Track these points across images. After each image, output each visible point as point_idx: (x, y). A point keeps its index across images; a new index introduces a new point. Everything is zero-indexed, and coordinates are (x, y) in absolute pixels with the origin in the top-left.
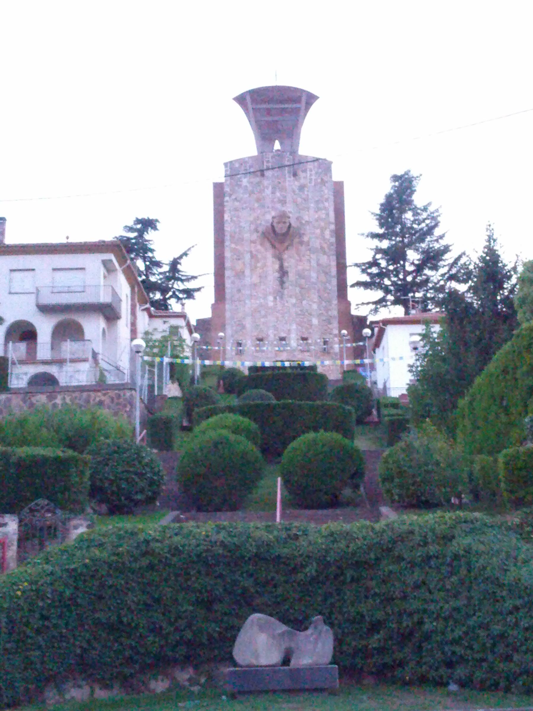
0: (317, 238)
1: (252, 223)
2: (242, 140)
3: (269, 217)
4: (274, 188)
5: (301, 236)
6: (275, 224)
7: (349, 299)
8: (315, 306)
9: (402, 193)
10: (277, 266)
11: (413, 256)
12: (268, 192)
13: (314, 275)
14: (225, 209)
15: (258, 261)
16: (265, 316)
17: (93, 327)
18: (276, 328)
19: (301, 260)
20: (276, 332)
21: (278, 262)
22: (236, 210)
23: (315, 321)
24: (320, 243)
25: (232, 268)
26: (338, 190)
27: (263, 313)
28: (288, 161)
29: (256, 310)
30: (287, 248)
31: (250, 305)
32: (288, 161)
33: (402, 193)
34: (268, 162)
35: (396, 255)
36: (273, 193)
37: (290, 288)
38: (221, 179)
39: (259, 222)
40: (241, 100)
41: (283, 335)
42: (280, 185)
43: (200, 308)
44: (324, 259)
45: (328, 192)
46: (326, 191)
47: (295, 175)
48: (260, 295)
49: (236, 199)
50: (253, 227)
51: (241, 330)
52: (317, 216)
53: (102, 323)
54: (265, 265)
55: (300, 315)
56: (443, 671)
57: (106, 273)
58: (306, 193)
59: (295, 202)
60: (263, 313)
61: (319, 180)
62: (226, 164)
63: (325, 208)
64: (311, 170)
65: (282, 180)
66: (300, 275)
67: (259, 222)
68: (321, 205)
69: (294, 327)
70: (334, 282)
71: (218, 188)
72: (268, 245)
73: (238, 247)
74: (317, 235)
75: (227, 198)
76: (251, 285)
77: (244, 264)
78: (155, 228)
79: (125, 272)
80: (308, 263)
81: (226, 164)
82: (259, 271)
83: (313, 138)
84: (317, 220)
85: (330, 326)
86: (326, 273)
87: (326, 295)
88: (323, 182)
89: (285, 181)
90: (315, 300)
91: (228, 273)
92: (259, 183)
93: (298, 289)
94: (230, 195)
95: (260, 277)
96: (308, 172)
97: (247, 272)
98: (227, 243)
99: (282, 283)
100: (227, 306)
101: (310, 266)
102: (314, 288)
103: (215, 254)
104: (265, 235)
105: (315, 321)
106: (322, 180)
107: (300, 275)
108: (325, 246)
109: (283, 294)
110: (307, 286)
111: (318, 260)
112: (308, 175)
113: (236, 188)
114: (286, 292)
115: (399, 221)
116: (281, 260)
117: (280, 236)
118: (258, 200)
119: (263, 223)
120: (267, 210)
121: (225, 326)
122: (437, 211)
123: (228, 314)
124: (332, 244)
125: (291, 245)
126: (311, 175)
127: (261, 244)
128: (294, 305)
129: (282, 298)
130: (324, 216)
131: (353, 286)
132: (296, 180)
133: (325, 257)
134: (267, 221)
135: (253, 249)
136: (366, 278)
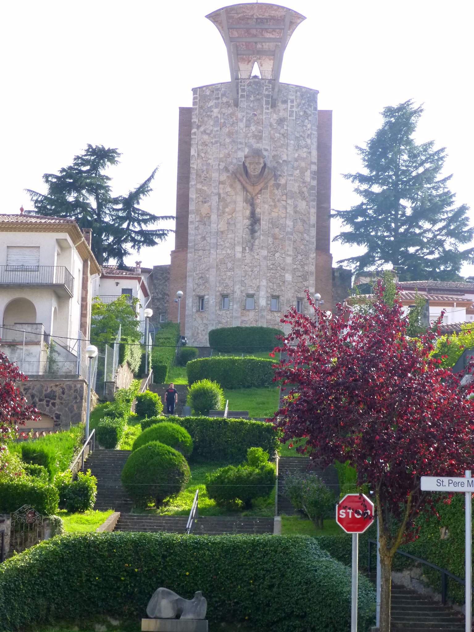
0: (295, 181)
1: (221, 160)
2: (215, 66)
3: (241, 155)
4: (248, 120)
5: (276, 177)
6: (247, 164)
7: (331, 251)
8: (289, 260)
9: (399, 123)
10: (248, 213)
11: (407, 205)
12: (242, 125)
13: (289, 223)
14: (192, 142)
15: (226, 206)
16: (232, 269)
17: (45, 306)
18: (242, 283)
19: (275, 206)
20: (243, 288)
21: (250, 208)
22: (205, 144)
23: (288, 277)
24: (299, 186)
25: (198, 212)
26: (324, 121)
27: (229, 265)
28: (267, 89)
29: (222, 262)
30: (260, 192)
31: (214, 257)
32: (267, 89)
33: (399, 123)
34: (243, 90)
35: (386, 204)
36: (247, 126)
37: (261, 238)
38: (189, 104)
39: (229, 160)
40: (214, 17)
41: (251, 292)
42: (255, 118)
43: (159, 255)
44: (302, 205)
45: (310, 127)
46: (309, 126)
47: (274, 105)
48: (227, 245)
49: (205, 131)
50: (222, 165)
51: (204, 284)
52: (296, 155)
53: (54, 304)
54: (234, 211)
55: (272, 269)
56: (449, 522)
57: (59, 251)
58: (285, 128)
59: (272, 138)
60: (229, 265)
61: (301, 113)
62: (195, 90)
63: (307, 146)
64: (292, 101)
65: (259, 111)
66: (274, 223)
67: (229, 160)
68: (302, 143)
69: (264, 283)
70: (313, 232)
71: (185, 113)
72: (239, 186)
73: (205, 188)
74: (296, 178)
75: (194, 130)
76: (217, 233)
77: (210, 206)
78: (112, 160)
79: (78, 248)
80: (283, 210)
81: (195, 90)
82: (227, 217)
83: (298, 66)
84: (296, 160)
85: (306, 284)
86: (304, 221)
87: (302, 247)
88: (306, 115)
89: (262, 113)
90: (290, 253)
91: (192, 217)
92: (232, 115)
93: (270, 240)
94: (198, 127)
95: (228, 223)
96: (289, 104)
97: (214, 217)
98: (192, 183)
99: (253, 231)
100: (189, 255)
101: (286, 213)
102: (290, 239)
103: (178, 192)
104: (235, 175)
105: (288, 277)
106: (305, 112)
107: (274, 223)
108: (305, 189)
109: (253, 245)
110: (281, 236)
111: (296, 206)
112: (289, 107)
113: (206, 119)
114: (257, 242)
115: (393, 163)
116: (252, 204)
117: (254, 175)
118: (230, 134)
119: (235, 161)
120: (240, 146)
121: (186, 277)
122: (442, 150)
123: (190, 265)
124: (312, 188)
125: (266, 188)
126: (292, 107)
127: (231, 186)
128: (265, 258)
129: (251, 250)
130: (304, 155)
131: (335, 239)
132: (275, 112)
133: (304, 203)
134: (238, 159)
135: (221, 191)
136: (349, 229)
